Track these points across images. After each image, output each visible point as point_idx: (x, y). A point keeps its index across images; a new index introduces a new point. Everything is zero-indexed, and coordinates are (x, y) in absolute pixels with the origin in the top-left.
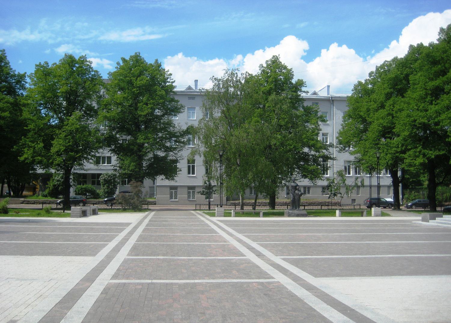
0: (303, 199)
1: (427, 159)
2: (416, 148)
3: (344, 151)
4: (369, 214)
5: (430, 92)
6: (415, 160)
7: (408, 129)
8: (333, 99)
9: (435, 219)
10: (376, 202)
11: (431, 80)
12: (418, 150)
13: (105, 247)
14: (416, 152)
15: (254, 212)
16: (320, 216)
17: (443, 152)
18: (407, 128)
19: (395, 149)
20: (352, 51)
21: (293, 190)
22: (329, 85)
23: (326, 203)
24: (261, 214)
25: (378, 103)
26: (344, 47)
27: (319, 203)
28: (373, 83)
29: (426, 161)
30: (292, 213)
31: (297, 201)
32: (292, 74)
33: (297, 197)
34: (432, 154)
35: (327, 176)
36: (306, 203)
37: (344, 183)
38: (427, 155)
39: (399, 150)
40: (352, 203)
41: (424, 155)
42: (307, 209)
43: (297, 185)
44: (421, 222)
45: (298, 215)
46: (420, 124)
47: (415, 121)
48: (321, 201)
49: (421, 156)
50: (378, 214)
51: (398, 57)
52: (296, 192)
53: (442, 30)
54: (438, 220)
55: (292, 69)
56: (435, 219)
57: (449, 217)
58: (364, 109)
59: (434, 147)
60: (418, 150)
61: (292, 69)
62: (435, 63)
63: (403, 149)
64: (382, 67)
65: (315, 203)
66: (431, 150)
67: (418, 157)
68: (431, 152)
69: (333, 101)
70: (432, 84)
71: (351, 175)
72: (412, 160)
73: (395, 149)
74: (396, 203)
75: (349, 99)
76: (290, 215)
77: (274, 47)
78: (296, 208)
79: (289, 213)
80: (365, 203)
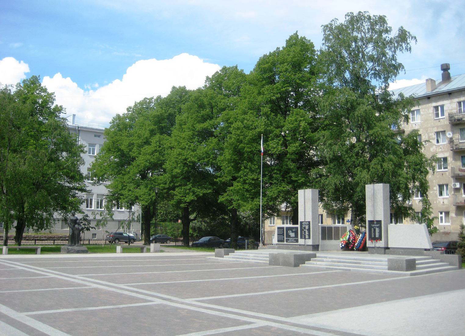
0: (86, 235)
1: (196, 196)
2: (186, 185)
3: (98, 184)
4: (148, 251)
5: (197, 133)
6: (185, 197)
7: (180, 167)
8: (79, 129)
9: (229, 255)
10: (117, 238)
11: (199, 122)
12: (188, 187)
13: (350, 307)
14: (186, 190)
15: (19, 249)
16: (100, 252)
17: (210, 191)
18: (179, 165)
19: (163, 185)
20: (75, 84)
21: (72, 224)
22: (74, 114)
23: (66, 237)
24: (39, 250)
25: (142, 138)
26: (69, 79)
27: (59, 237)
28: (132, 119)
29: (196, 199)
30: (72, 249)
31: (76, 237)
32: (54, 98)
33: (76, 232)
34: (201, 192)
35: (101, 209)
36: (45, 237)
37: (111, 217)
38: (196, 192)
39: (167, 186)
40: (92, 238)
41: (194, 193)
42: (38, 244)
43: (77, 219)
44: (214, 257)
45: (78, 252)
46: (190, 162)
47: (186, 159)
48: (61, 235)
49: (191, 194)
50: (158, 250)
51: (162, 97)
52: (76, 226)
53: (208, 78)
54: (231, 255)
55: (54, 93)
56: (229, 255)
57: (241, 253)
58: (126, 143)
59: (201, 185)
60: (188, 187)
61: (54, 93)
62: (202, 106)
63: (171, 186)
64: (141, 103)
65: (54, 237)
66: (199, 189)
67: (188, 194)
68: (199, 190)
69: (79, 130)
70: (199, 126)
71: (93, 209)
72: (183, 196)
73: (163, 185)
74: (147, 239)
75: (107, 132)
76: (69, 252)
77: (126, 73)
78: (75, 244)
79: (68, 249)
80: (108, 238)
